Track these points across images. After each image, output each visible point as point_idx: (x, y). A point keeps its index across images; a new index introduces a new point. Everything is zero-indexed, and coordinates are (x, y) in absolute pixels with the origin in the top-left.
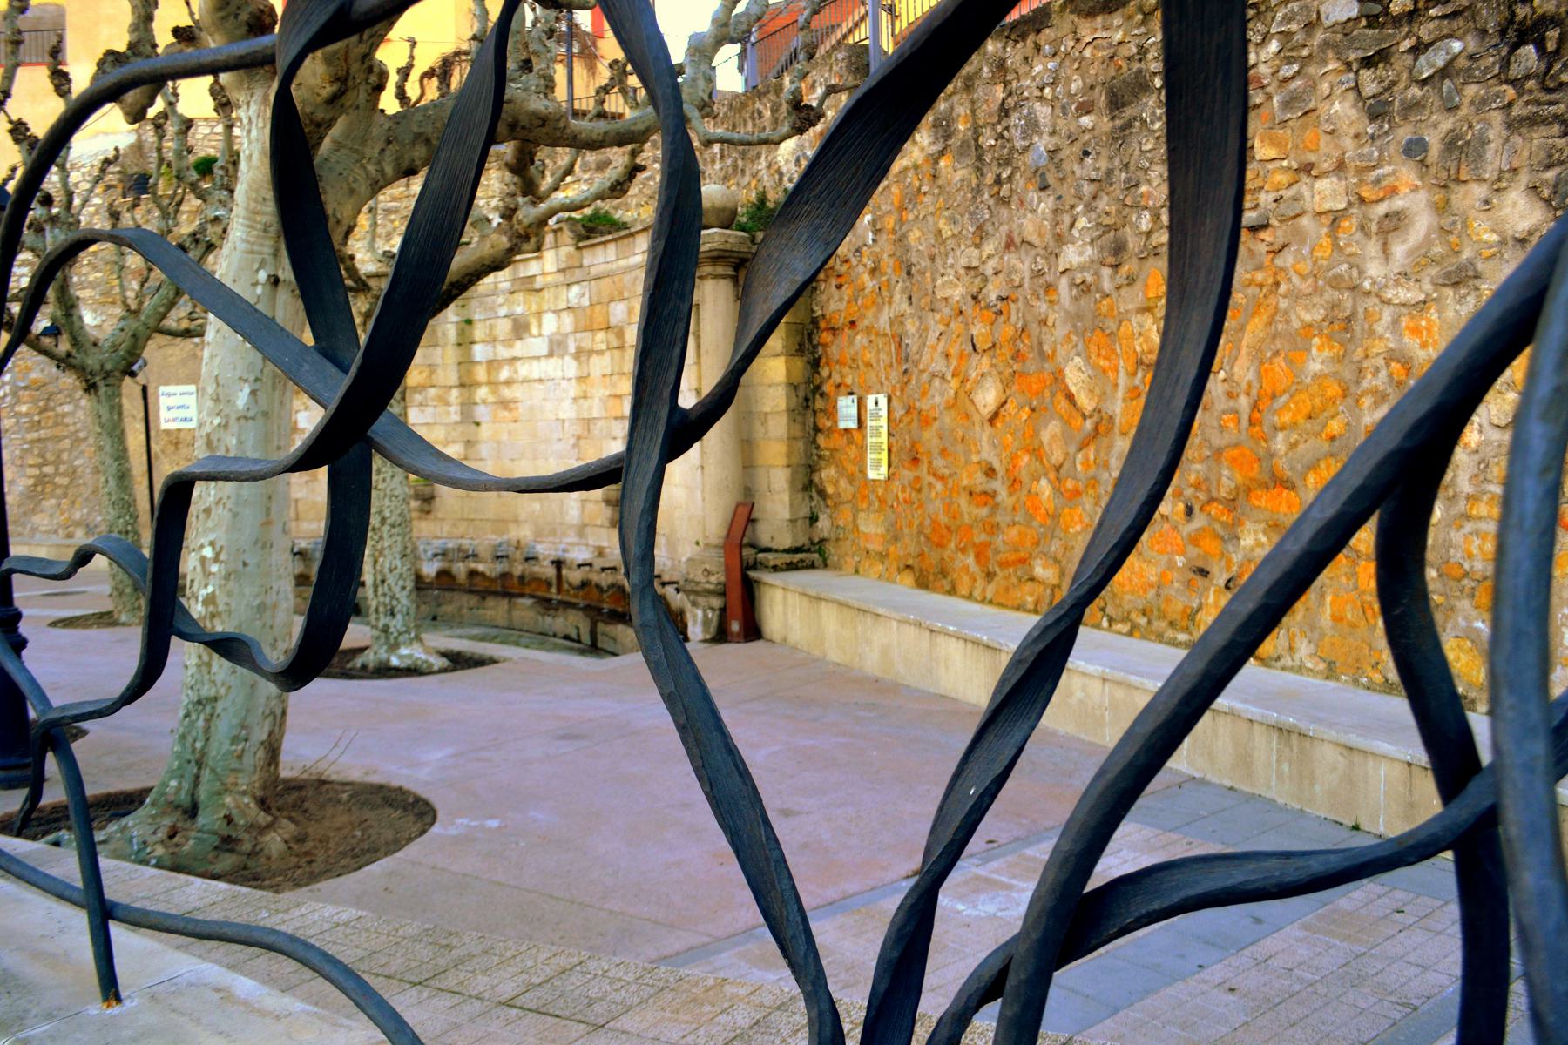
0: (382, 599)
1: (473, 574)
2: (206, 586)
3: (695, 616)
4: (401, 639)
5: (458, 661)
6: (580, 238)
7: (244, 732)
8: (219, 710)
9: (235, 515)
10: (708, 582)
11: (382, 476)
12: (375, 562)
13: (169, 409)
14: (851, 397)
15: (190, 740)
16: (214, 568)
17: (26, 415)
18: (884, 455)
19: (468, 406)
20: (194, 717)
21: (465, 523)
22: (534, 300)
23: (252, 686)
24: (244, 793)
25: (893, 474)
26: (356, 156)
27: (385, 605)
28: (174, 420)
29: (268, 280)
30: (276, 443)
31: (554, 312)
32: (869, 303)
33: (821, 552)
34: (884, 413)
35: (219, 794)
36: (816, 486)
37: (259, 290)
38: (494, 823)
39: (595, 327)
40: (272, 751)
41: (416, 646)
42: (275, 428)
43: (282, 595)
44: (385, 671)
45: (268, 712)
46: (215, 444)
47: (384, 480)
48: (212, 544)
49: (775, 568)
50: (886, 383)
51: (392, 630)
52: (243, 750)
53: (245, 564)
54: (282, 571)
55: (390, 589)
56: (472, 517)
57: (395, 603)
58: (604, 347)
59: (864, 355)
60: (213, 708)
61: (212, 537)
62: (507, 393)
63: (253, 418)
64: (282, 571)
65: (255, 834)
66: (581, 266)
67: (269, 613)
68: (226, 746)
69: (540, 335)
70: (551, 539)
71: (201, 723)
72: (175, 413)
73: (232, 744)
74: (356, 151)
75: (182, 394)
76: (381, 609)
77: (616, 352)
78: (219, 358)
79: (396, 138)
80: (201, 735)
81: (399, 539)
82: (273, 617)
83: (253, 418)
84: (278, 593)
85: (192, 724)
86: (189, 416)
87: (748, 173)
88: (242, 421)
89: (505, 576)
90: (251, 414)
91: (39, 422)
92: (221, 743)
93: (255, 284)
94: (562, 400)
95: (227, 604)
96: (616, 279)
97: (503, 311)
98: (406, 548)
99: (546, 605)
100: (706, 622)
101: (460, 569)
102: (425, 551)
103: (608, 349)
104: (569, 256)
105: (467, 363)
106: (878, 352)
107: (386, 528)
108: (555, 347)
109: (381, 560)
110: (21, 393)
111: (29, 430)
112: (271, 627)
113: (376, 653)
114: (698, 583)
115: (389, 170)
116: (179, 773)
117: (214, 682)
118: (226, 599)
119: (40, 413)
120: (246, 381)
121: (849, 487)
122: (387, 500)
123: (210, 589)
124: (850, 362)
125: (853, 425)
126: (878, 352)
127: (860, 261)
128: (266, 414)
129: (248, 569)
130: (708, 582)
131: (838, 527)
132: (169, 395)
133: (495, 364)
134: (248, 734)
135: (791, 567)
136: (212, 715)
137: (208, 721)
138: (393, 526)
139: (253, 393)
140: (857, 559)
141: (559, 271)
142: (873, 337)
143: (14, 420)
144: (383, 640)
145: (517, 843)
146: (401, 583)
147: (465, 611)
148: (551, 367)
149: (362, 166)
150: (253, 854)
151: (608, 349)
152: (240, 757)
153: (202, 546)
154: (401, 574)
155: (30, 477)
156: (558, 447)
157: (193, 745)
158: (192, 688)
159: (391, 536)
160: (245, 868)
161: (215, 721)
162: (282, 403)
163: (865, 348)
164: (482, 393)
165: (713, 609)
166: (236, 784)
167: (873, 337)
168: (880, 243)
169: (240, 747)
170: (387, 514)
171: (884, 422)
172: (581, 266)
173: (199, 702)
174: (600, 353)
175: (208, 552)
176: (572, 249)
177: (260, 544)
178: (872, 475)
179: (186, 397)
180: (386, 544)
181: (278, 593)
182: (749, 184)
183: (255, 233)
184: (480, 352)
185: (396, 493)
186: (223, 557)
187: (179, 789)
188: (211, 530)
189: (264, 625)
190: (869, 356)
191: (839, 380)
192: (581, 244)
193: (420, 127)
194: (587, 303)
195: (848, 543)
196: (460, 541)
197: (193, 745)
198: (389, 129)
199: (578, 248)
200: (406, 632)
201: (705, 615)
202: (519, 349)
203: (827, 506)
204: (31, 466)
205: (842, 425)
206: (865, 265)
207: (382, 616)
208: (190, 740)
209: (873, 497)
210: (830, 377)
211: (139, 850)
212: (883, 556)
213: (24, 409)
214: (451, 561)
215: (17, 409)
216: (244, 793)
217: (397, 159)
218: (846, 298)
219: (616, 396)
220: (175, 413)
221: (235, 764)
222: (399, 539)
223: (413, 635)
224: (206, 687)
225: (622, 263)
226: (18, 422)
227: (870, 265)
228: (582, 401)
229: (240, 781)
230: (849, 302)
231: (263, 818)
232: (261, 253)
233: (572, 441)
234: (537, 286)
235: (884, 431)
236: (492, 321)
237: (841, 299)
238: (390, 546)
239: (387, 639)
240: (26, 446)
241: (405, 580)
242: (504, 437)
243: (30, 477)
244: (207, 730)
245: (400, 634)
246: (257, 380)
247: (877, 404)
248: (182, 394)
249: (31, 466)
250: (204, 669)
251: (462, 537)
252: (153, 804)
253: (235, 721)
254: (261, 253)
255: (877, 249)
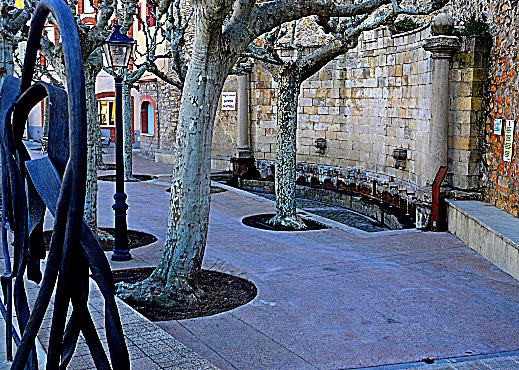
0: (280, 196)
1: (339, 182)
2: (176, 197)
3: (419, 216)
4: (287, 213)
5: (311, 225)
6: (393, 33)
7: (185, 254)
8: (177, 245)
9: (186, 171)
10: (426, 202)
11: (284, 144)
12: (279, 180)
13: (225, 101)
14: (500, 120)
15: (167, 255)
16: (179, 190)
17: (173, 101)
18: (511, 150)
19: (342, 107)
20: (169, 246)
21: (338, 160)
22: (373, 60)
23: (189, 237)
24: (183, 278)
25: (514, 160)
26: (244, 25)
27: (282, 198)
28: (226, 106)
29: (203, 79)
30: (204, 143)
31: (380, 67)
32: (511, 74)
33: (483, 192)
34: (512, 129)
35: (174, 276)
36: (483, 160)
37: (199, 83)
38: (273, 304)
39: (397, 75)
40: (198, 262)
41: (293, 217)
42: (204, 138)
43: (204, 203)
44: (278, 227)
45: (195, 247)
46: (181, 143)
47: (285, 146)
48: (179, 181)
49: (458, 199)
50: (515, 114)
51: (284, 209)
52: (184, 261)
53: (189, 190)
54: (204, 193)
55: (284, 192)
56: (341, 157)
57: (285, 198)
58: (400, 85)
59: (507, 100)
60: (175, 244)
61: (179, 179)
62: (358, 102)
63: (195, 134)
64: (204, 193)
65: (184, 294)
66: (393, 46)
67: (198, 209)
68: (178, 259)
69: (374, 77)
70: (373, 171)
71: (171, 249)
72: (227, 104)
73: (180, 258)
74: (244, 23)
75: (230, 96)
76: (280, 200)
77: (405, 87)
78: (184, 110)
79: (261, 17)
80: (171, 253)
81: (289, 171)
82: (199, 211)
83: (195, 134)
84: (202, 202)
85: (169, 248)
86: (232, 105)
87: (470, 4)
88: (191, 135)
89: (352, 185)
90: (194, 132)
91: (177, 104)
92: (177, 258)
93: (198, 81)
94: (381, 108)
95: (182, 205)
96: (407, 53)
97: (359, 66)
98: (292, 175)
99: (366, 200)
100: (424, 220)
101: (334, 180)
102: (321, 171)
103: (402, 86)
104: (388, 41)
105: (343, 88)
106: (513, 99)
107: (284, 166)
108: (380, 83)
109: (281, 179)
110: (171, 92)
111: (174, 108)
112: (198, 215)
113: (276, 218)
114: (421, 201)
115: (258, 31)
116: (162, 266)
117: (176, 234)
118: (182, 203)
119: (178, 101)
120: (193, 119)
121: (496, 163)
122: (285, 154)
123: (177, 198)
124: (501, 102)
125: (499, 133)
126: (513, 99)
127: (509, 53)
128: (200, 132)
129: (190, 192)
130: (426, 202)
131: (490, 181)
132: (225, 96)
133: (355, 90)
134: (186, 255)
135: (466, 198)
136: (175, 246)
137: (173, 248)
138: (287, 166)
139: (195, 124)
140: (496, 198)
141: (384, 48)
142: (511, 91)
143: (168, 103)
144: (280, 213)
145: (275, 315)
146: (289, 190)
147: (333, 199)
148: (376, 92)
149: (247, 30)
150: (182, 302)
151: (402, 86)
152: (183, 264)
153: (175, 182)
154: (289, 186)
155: (173, 126)
156: (378, 129)
157: (168, 257)
158: (169, 235)
159: (286, 170)
160: (179, 306)
161: (175, 249)
162: (207, 128)
163: (508, 96)
164: (348, 102)
165: (427, 215)
166: (180, 274)
167: (511, 91)
168: (517, 45)
169: (183, 260)
170: (285, 160)
171: (512, 134)
172: (393, 46)
173: (171, 241)
174: (398, 87)
175: (177, 184)
176: (390, 38)
177: (195, 183)
178: (505, 159)
179: (232, 97)
180: (284, 173)
181: (202, 202)
182: (470, 8)
183: (198, 61)
184: (348, 83)
185: (289, 152)
186: (182, 187)
187: (161, 272)
188: (179, 176)
189: (195, 214)
190: (510, 100)
191: (496, 111)
192: (393, 36)
193: (271, 12)
194: (394, 64)
195: (494, 190)
196: (335, 167)
197: (168, 257)
198: (258, 13)
199: (392, 38)
200: (289, 211)
201: (423, 216)
202: (365, 82)
203: (487, 171)
204: (174, 122)
205: (495, 133)
206: (511, 55)
207: (280, 203)
208: (167, 255)
209: (505, 169)
210: (493, 108)
211: (143, 294)
212: (507, 199)
213: (172, 98)
214: (331, 176)
215: (170, 98)
216: (183, 278)
217: (261, 26)
218: (503, 70)
219: (403, 108)
220: (227, 104)
221: (181, 266)
222: (289, 171)
223: (292, 212)
224: (174, 235)
225: (410, 46)
226: (170, 104)
227: (513, 55)
228: (389, 109)
229: (182, 273)
230: (504, 72)
231: (189, 288)
232: (200, 69)
233: (384, 127)
234: (374, 55)
235: (512, 138)
236: (355, 70)
237: (501, 70)
238: (285, 174)
239: (282, 213)
240: (172, 114)
241: (290, 189)
242: (357, 123)
243: (173, 126)
244: (173, 252)
245: (287, 211)
246: (197, 119)
247: (510, 123)
248: (230, 96)
249: (174, 122)
250: (173, 228)
251: (336, 166)
252: (153, 277)
253: (182, 250)
254: (200, 69)
255: (516, 48)
